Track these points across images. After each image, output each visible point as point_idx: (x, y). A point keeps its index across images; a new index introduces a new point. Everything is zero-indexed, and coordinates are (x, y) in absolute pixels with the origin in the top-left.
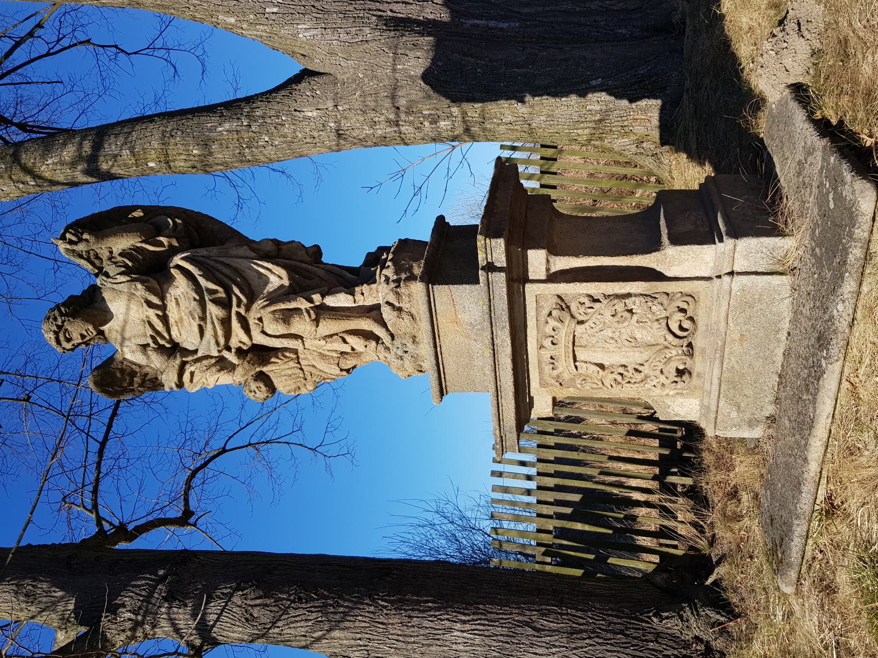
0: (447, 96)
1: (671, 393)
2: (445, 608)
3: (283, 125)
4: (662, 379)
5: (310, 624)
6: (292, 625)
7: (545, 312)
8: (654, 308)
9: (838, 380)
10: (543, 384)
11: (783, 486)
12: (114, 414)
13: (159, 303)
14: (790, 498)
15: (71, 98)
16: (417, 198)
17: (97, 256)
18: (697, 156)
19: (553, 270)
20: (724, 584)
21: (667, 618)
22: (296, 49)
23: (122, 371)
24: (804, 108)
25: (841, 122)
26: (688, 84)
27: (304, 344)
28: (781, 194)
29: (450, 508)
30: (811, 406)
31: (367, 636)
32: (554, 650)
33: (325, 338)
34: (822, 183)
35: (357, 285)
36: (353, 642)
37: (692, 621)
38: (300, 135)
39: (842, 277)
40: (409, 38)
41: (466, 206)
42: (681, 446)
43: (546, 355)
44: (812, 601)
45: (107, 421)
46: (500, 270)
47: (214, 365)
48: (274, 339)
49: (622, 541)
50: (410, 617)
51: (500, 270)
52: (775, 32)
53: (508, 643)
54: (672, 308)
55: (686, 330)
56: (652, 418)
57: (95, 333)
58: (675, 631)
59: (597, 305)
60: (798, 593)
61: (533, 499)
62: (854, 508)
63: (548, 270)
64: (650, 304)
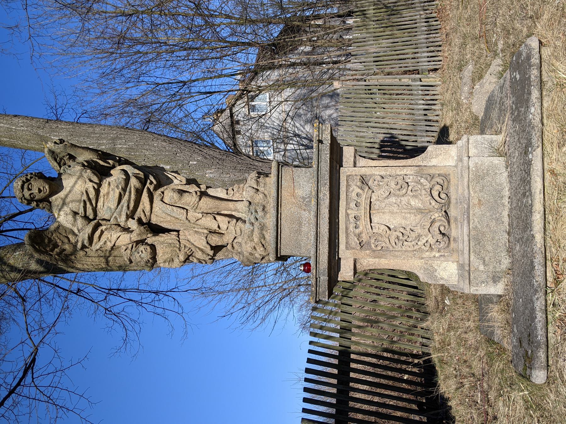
8: (422, 181)
13: (97, 182)
27: (187, 214)
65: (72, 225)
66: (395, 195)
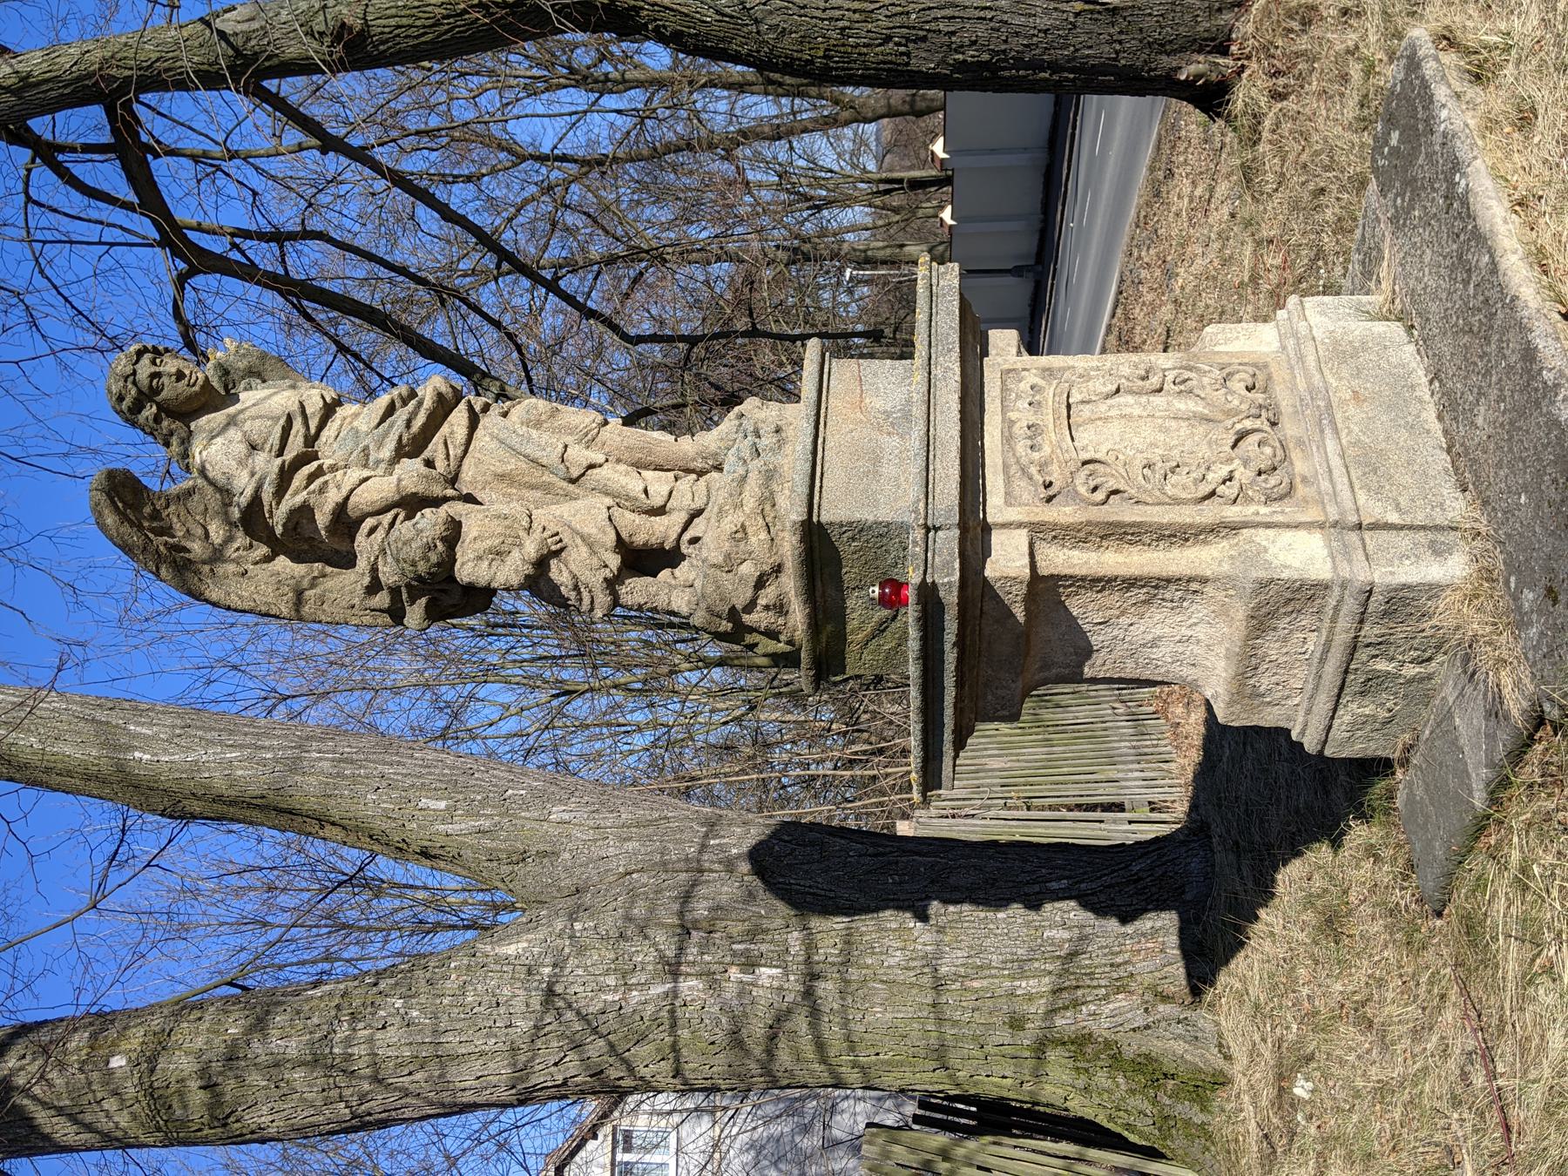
65: (240, 463)
66: (1131, 392)
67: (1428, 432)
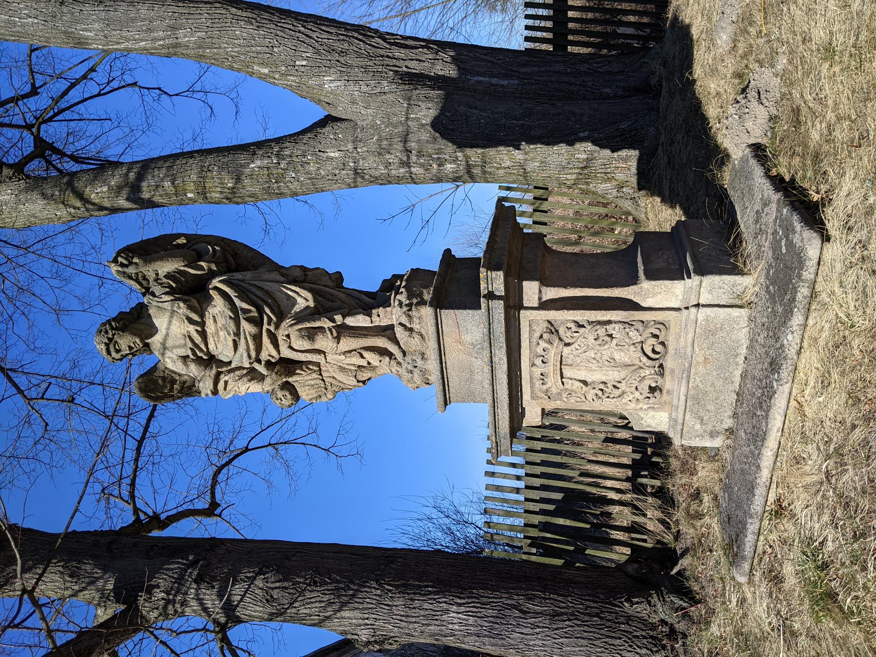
0: (454, 142)
1: (645, 407)
2: (443, 592)
3: (308, 163)
4: (637, 394)
5: (323, 605)
6: (307, 606)
7: (537, 335)
8: (631, 333)
9: (787, 400)
10: (534, 397)
11: (739, 489)
12: (151, 416)
14: (745, 499)
15: (116, 134)
16: (425, 231)
17: (144, 278)
18: (670, 200)
19: (544, 299)
20: (687, 573)
21: (637, 603)
22: (322, 98)
23: (164, 379)
24: (763, 165)
25: (793, 180)
26: (663, 138)
28: (741, 238)
29: (446, 504)
30: (764, 421)
31: (374, 616)
32: (538, 630)
33: (345, 353)
34: (776, 230)
35: (374, 308)
36: (361, 622)
37: (659, 606)
38: (323, 173)
39: (792, 312)
40: (422, 92)
41: (471, 243)
42: (651, 454)
43: (537, 371)
44: (762, 589)
45: (144, 422)
46: (499, 298)
47: (245, 375)
48: (299, 354)
49: (597, 535)
50: (412, 600)
51: (499, 298)
52: (738, 98)
53: (498, 624)
54: (647, 334)
55: (659, 353)
56: (627, 427)
57: (141, 345)
58: (644, 614)
59: (582, 330)
60: (750, 582)
61: (521, 498)
62: (799, 509)
63: (540, 299)
64: (627, 330)
67: (733, 382)
